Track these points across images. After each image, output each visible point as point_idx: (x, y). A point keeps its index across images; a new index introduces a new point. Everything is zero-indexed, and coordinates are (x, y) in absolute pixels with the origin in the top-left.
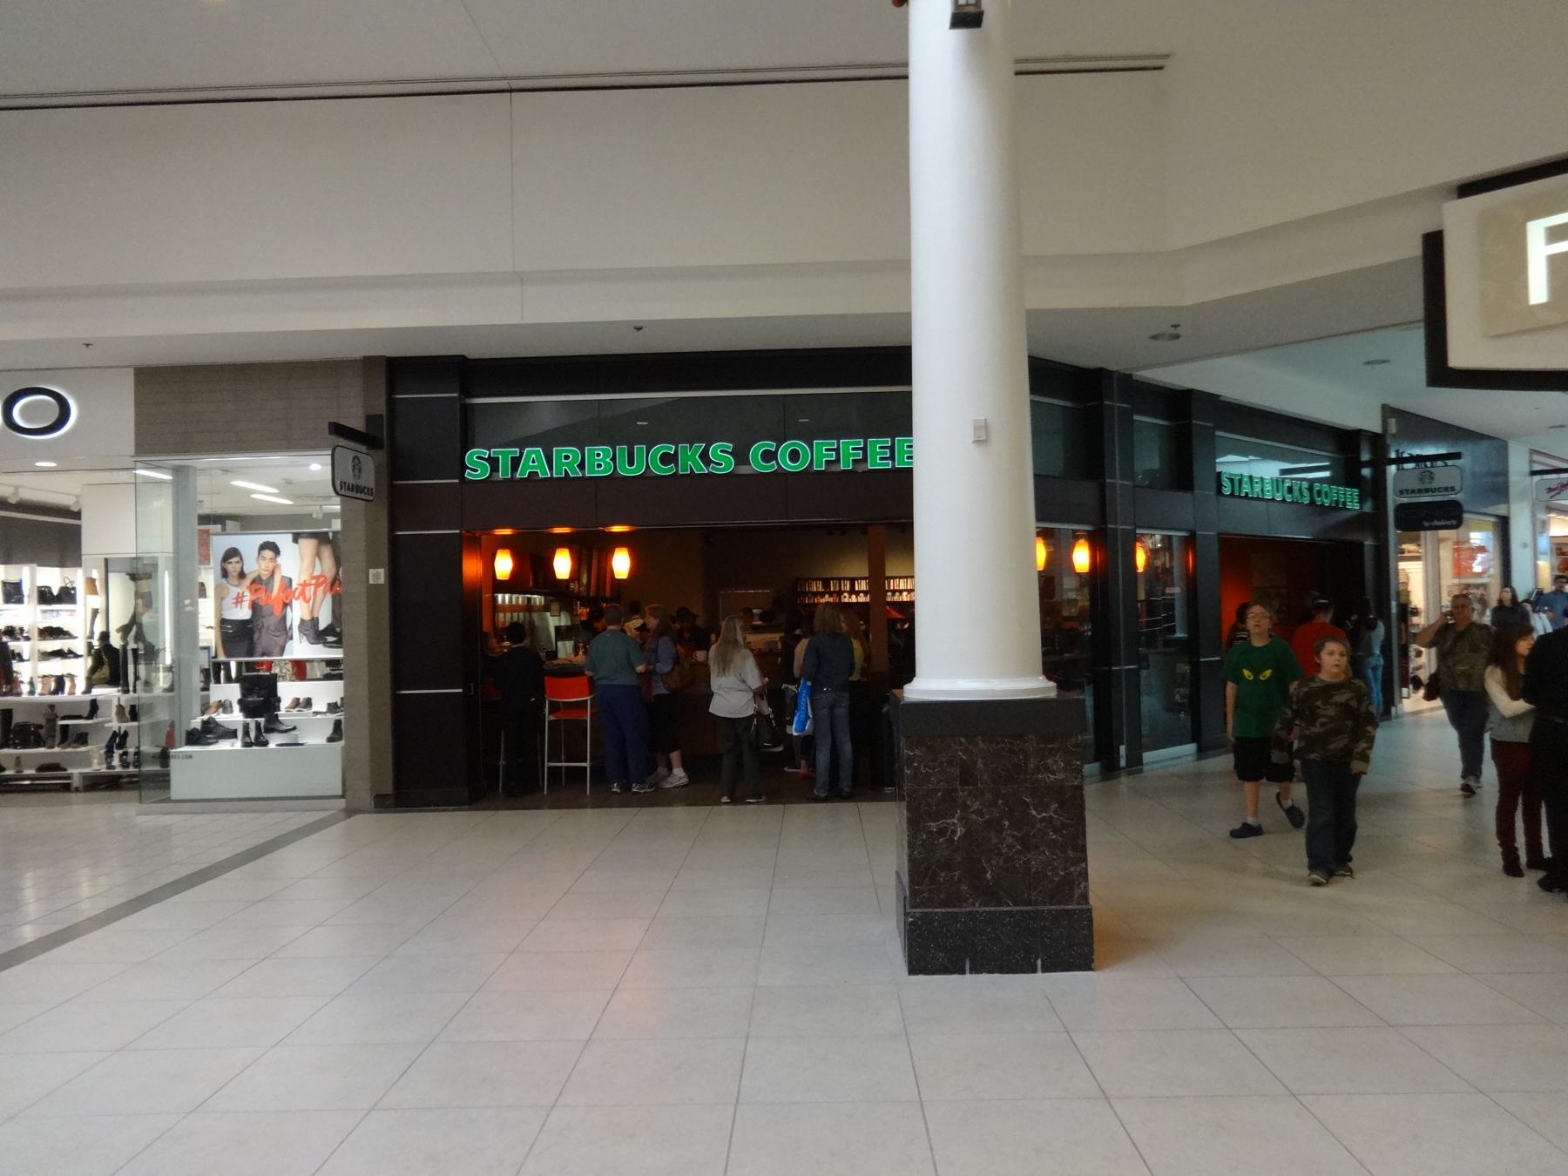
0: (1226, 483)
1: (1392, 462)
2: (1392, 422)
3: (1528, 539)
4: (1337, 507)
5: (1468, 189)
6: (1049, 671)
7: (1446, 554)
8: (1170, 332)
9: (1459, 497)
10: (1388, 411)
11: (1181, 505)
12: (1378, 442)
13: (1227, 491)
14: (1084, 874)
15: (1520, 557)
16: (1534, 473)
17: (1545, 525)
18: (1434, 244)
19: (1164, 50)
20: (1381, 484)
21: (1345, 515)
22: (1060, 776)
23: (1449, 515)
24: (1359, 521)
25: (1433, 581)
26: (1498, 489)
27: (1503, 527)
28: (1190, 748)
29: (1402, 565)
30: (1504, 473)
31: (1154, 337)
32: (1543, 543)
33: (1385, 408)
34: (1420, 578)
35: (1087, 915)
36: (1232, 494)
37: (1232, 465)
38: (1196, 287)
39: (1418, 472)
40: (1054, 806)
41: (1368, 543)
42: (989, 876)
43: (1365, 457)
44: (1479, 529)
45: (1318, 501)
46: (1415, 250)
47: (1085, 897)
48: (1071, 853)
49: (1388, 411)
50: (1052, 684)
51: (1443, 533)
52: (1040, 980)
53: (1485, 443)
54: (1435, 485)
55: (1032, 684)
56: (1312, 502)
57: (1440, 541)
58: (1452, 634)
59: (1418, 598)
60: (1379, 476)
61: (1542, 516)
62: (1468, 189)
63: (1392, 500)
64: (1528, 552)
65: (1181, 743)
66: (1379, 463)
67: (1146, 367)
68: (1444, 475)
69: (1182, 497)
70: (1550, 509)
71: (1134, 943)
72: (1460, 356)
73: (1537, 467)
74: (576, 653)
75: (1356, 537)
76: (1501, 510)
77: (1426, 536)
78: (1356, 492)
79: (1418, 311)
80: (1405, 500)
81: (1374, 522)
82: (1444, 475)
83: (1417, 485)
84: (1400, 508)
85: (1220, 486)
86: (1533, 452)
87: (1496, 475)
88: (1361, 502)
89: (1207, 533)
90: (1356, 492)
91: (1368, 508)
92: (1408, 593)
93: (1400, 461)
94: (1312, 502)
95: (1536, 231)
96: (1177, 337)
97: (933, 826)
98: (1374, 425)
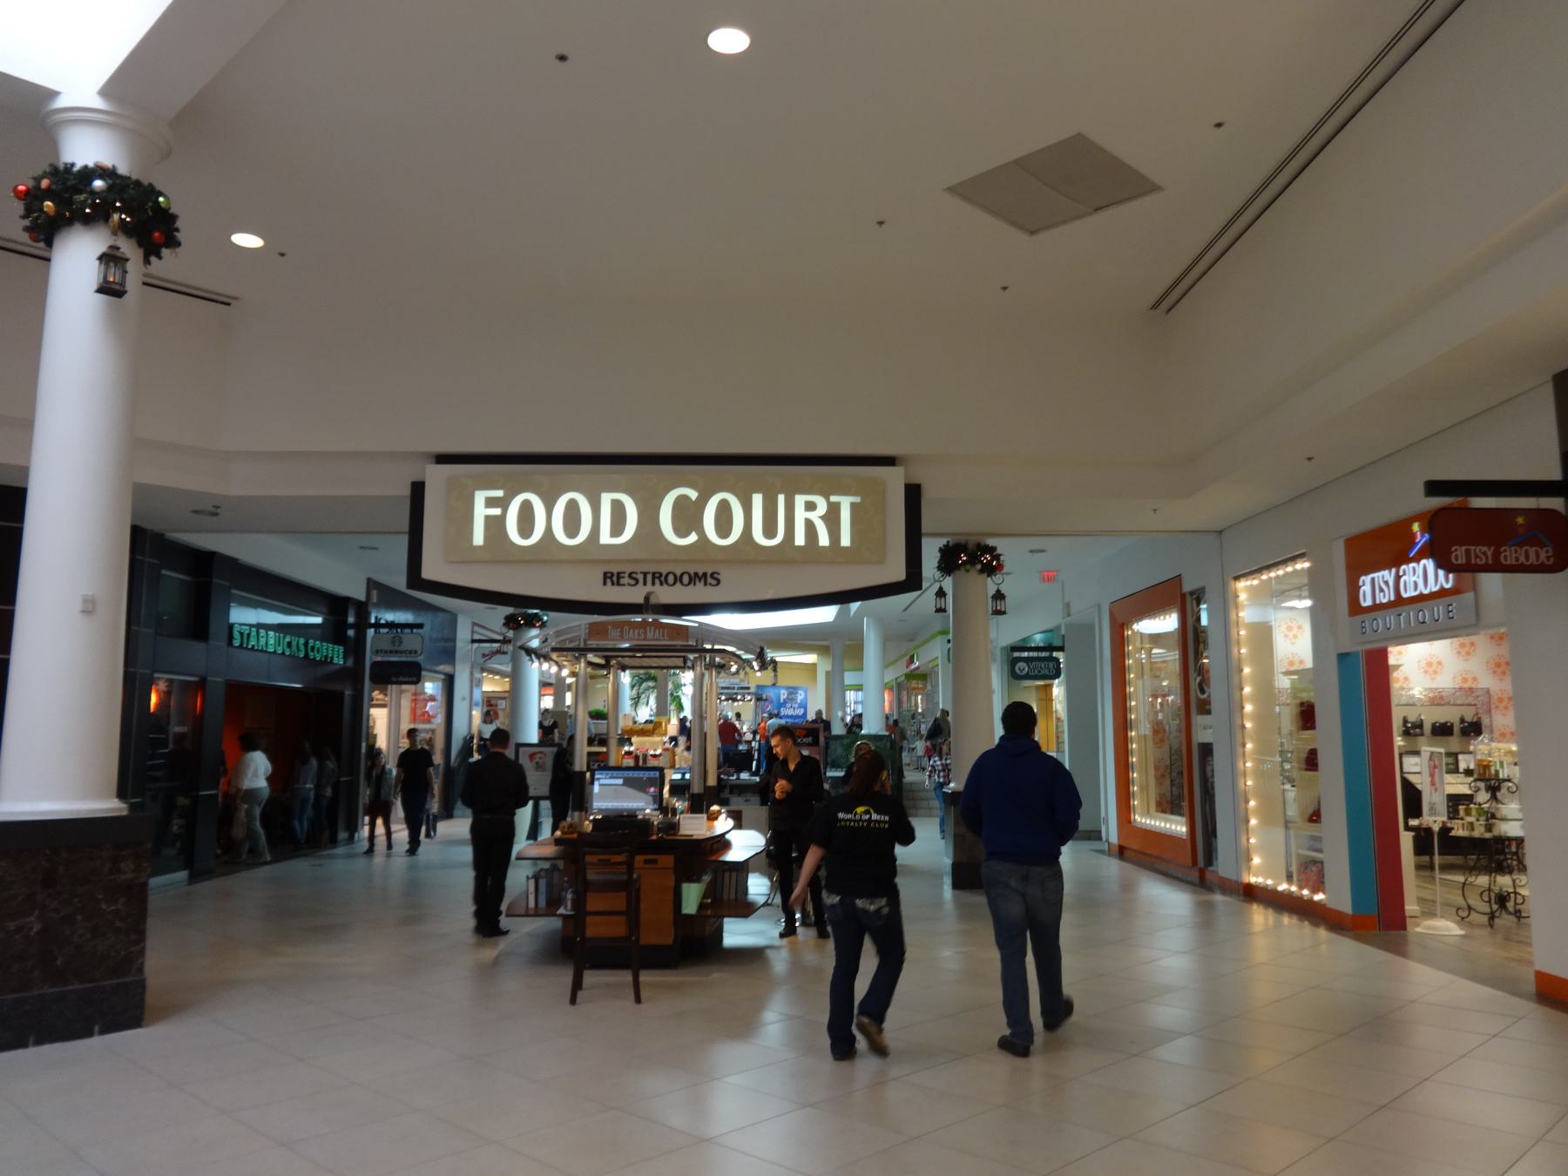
0: (236, 635)
1: (372, 626)
2: (374, 593)
3: (466, 693)
4: (326, 661)
5: (442, 459)
6: (121, 794)
7: (406, 704)
8: (211, 511)
9: (420, 659)
10: (372, 584)
11: (195, 655)
12: (362, 608)
13: (236, 643)
14: (142, 952)
15: (460, 707)
16: (474, 641)
17: (479, 683)
18: (418, 489)
19: (234, 294)
20: (360, 645)
21: (332, 668)
22: (129, 876)
23: (411, 673)
24: (342, 674)
25: (394, 722)
26: (449, 654)
27: (449, 683)
28: (183, 875)
29: (373, 711)
30: (453, 640)
31: (195, 512)
32: (477, 695)
33: (369, 581)
34: (384, 723)
35: (141, 986)
36: (241, 646)
37: (242, 616)
38: (241, 484)
39: (390, 636)
40: (122, 900)
41: (348, 692)
42: (59, 962)
43: (351, 620)
44: (432, 680)
45: (311, 655)
46: (406, 491)
47: (141, 970)
48: (133, 937)
49: (372, 584)
50: (123, 805)
51: (404, 687)
52: (97, 1042)
53: (441, 614)
54: (403, 647)
55: (107, 805)
56: (307, 655)
57: (402, 692)
58: (415, 759)
59: (382, 742)
60: (361, 637)
61: (477, 675)
62: (442, 459)
63: (369, 658)
64: (466, 704)
65: (175, 871)
66: (362, 624)
67: (185, 531)
68: (410, 641)
69: (200, 646)
70: (483, 670)
71: (169, 1010)
72: (429, 572)
73: (477, 637)
74: (1287, 673)
75: (337, 687)
76: (446, 668)
77: (393, 688)
78: (342, 649)
79: (405, 524)
80: (379, 659)
81: (353, 675)
82: (410, 641)
83: (388, 647)
84: (374, 665)
85: (231, 638)
86: (474, 624)
87: (447, 640)
88: (345, 658)
89: (216, 679)
90: (342, 649)
91: (350, 663)
92: (375, 736)
93: (377, 625)
94: (307, 655)
95: (480, 497)
96: (215, 514)
97: (12, 926)
98: (359, 594)
